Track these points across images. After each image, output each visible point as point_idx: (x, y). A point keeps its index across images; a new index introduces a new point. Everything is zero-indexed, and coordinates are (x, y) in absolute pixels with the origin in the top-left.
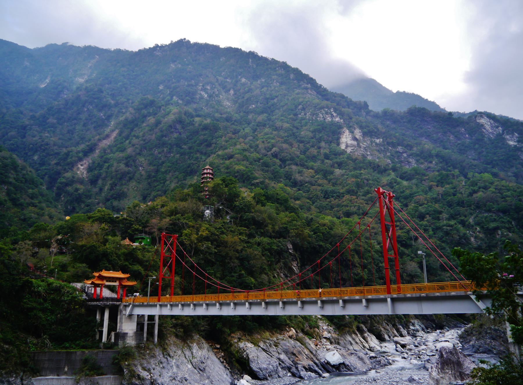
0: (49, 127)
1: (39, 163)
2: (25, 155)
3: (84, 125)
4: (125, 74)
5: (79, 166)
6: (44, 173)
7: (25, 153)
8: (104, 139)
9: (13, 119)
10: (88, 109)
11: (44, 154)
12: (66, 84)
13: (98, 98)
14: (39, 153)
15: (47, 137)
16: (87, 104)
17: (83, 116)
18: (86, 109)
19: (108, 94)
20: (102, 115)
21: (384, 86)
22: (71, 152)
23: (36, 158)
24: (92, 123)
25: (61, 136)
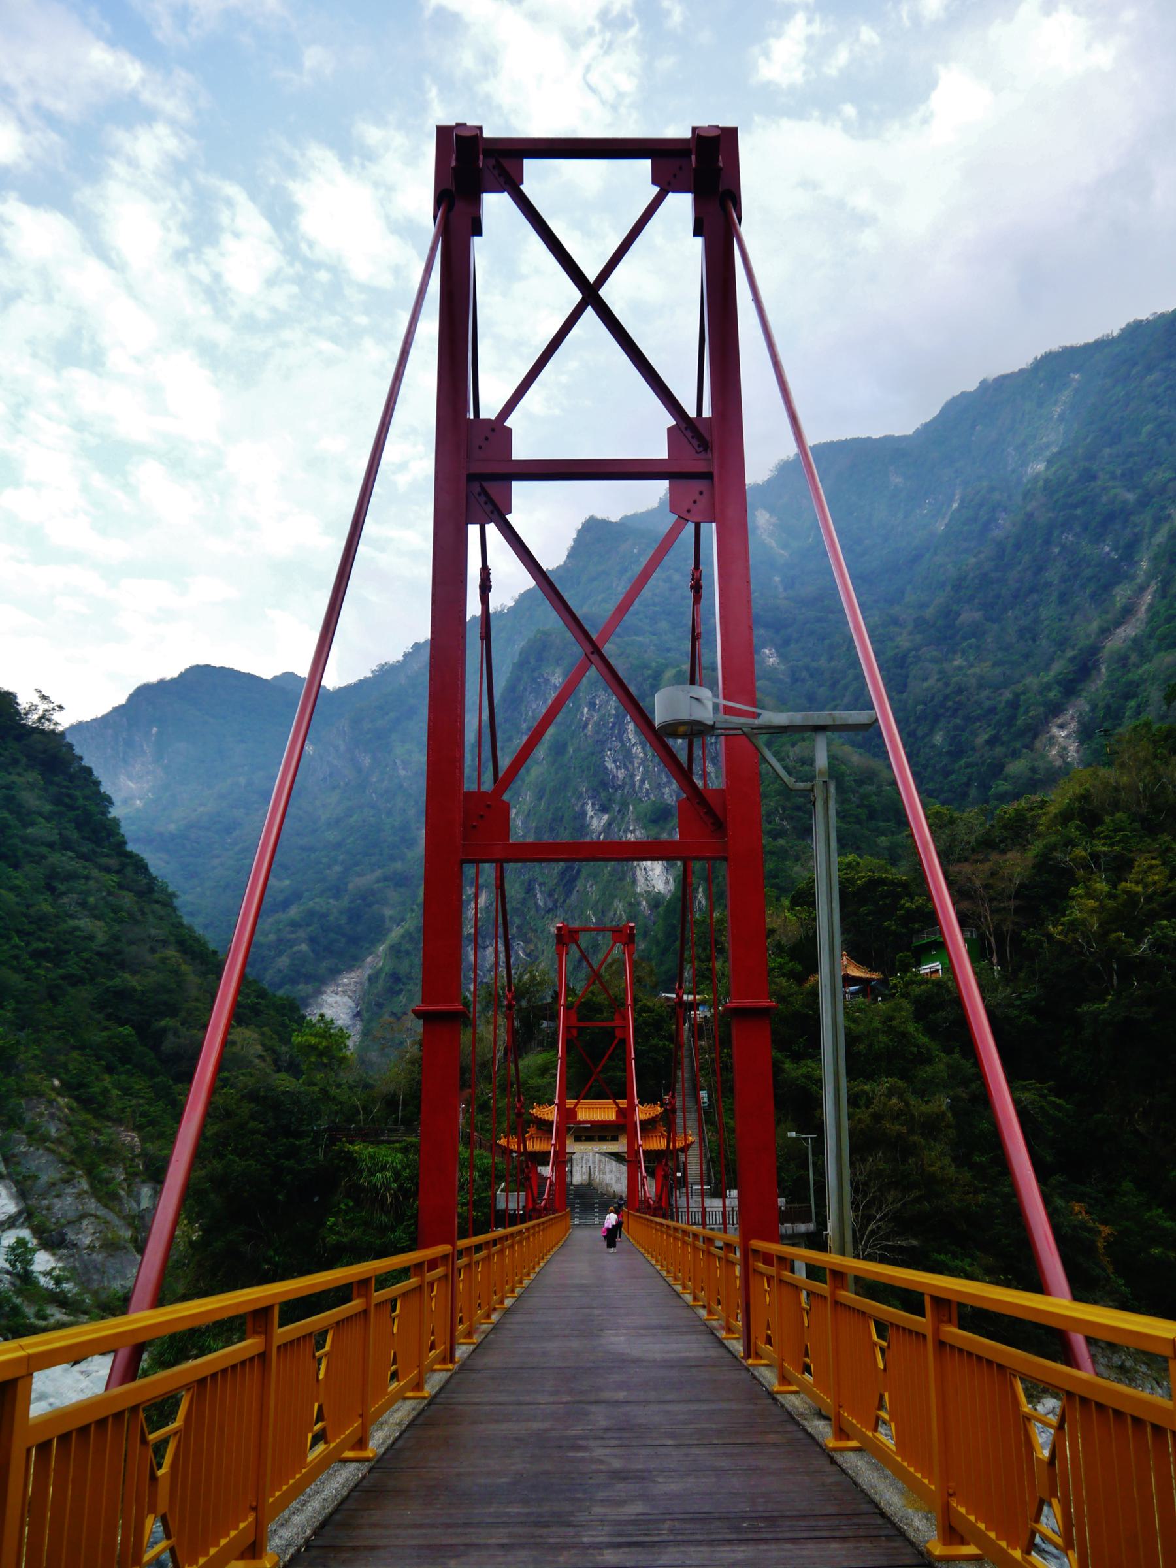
0: (965, 638)
1: (949, 753)
3: (1063, 599)
4: (1160, 390)
5: (1055, 731)
6: (965, 779)
8: (1118, 624)
10: (1063, 547)
11: (958, 721)
12: (996, 496)
13: (1084, 502)
14: (943, 723)
15: (960, 668)
16: (1056, 533)
17: (1052, 575)
18: (1057, 550)
19: (1113, 477)
20: (1107, 549)
21: (876, 435)
22: (1023, 693)
23: (938, 738)
24: (1083, 587)
25: (1000, 655)
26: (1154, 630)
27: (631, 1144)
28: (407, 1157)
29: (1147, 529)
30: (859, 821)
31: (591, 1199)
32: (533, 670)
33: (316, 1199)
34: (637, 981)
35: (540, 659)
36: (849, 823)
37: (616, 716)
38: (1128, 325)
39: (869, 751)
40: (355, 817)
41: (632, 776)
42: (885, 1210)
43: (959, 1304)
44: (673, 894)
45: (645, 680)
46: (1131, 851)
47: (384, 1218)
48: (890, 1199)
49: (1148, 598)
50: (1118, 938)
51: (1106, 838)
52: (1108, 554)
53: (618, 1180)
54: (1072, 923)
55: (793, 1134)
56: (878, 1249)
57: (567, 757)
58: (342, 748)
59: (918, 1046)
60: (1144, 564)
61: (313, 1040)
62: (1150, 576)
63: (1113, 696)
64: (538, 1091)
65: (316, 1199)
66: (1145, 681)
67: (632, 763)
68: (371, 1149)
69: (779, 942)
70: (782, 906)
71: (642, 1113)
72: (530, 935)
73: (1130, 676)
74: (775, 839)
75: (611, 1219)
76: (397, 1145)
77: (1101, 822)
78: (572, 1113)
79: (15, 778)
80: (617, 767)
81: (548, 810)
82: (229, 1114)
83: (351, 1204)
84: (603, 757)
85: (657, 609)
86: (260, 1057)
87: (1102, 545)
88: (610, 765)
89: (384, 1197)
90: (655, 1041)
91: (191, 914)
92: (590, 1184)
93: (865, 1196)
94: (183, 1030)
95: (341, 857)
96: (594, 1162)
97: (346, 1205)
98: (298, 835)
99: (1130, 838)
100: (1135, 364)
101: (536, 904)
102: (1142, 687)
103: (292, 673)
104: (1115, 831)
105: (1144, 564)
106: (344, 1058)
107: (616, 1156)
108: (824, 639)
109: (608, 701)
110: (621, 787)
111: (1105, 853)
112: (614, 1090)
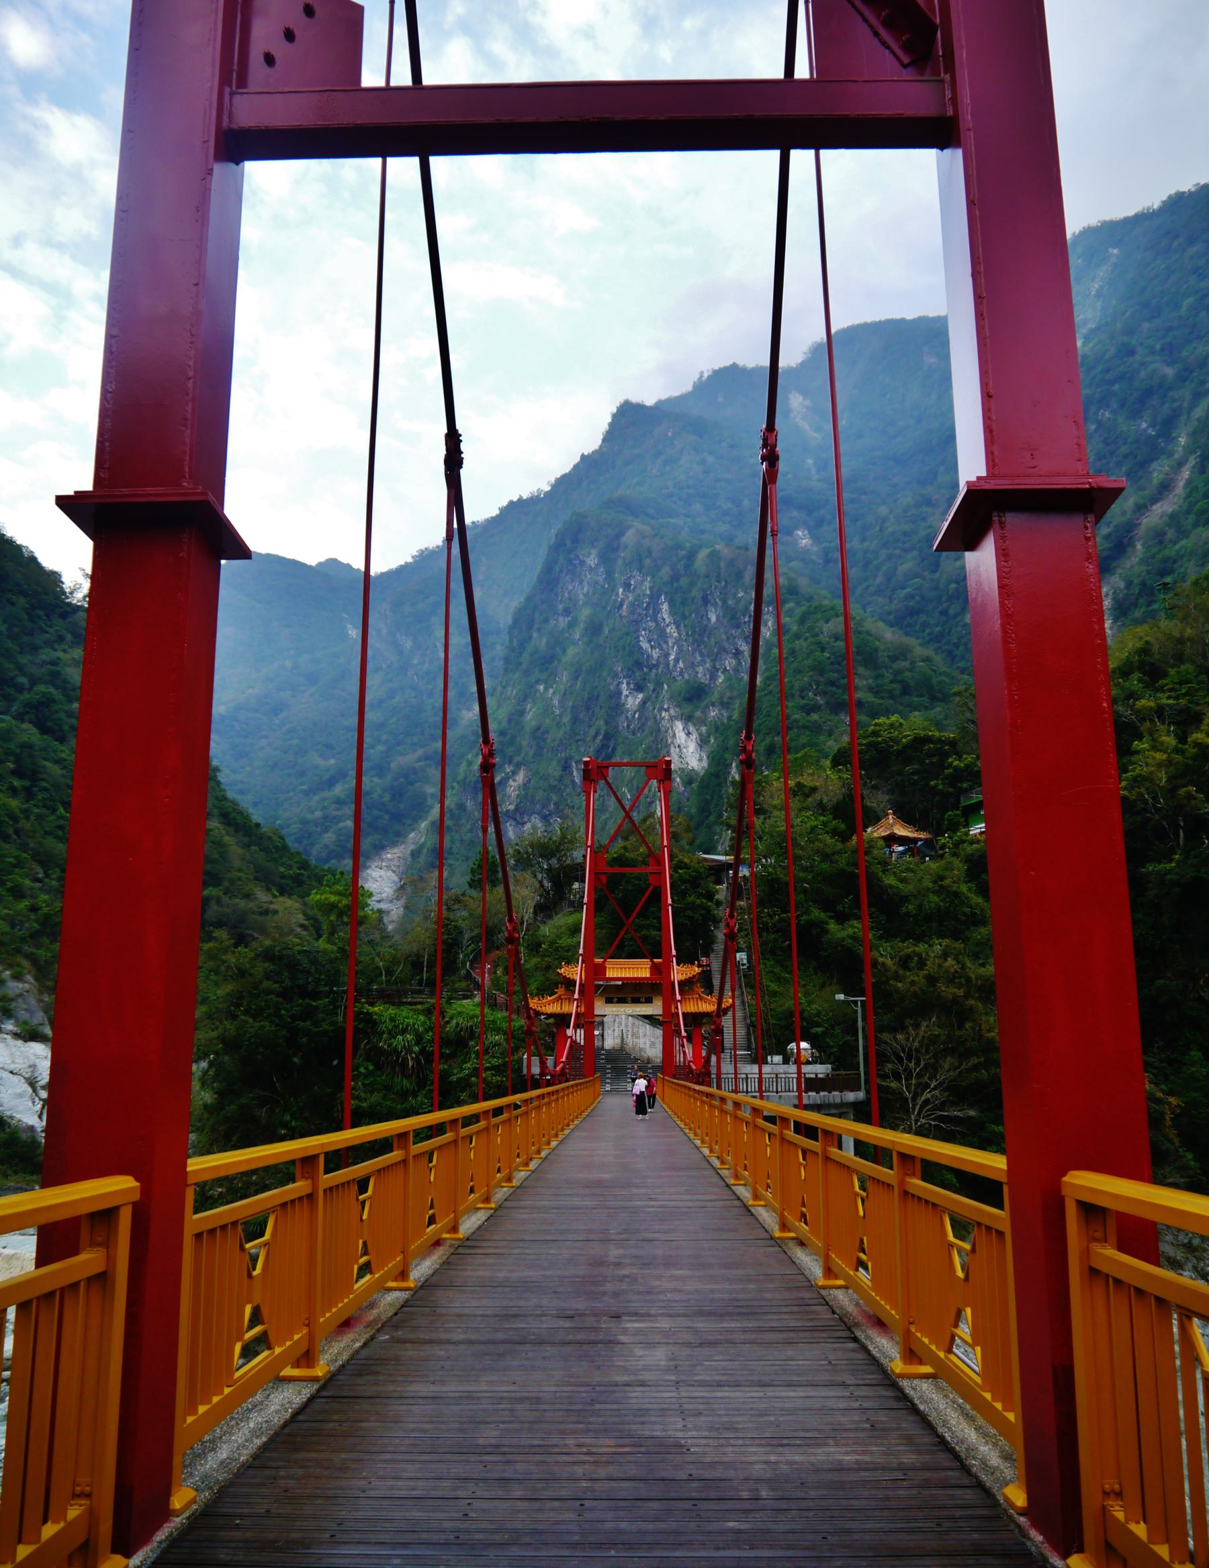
2: (944, 618)
7: (942, 613)
8: (1154, 500)
9: (906, 527)
10: (1100, 424)
13: (1121, 377)
16: (1093, 409)
18: (1093, 427)
19: (1152, 352)
20: (1144, 425)
21: (910, 316)
24: (1119, 464)
26: (1192, 505)
27: (666, 1007)
28: (430, 1019)
29: (1185, 405)
30: (892, 697)
31: (621, 1064)
32: (569, 552)
33: (335, 1063)
34: (674, 837)
35: (576, 541)
36: (883, 698)
37: (651, 597)
38: (1170, 197)
39: (901, 629)
40: (398, 698)
41: (667, 655)
42: (941, 1077)
43: (923, 1160)
44: (707, 771)
45: (679, 560)
46: (1198, 704)
47: (405, 1081)
48: (947, 1066)
49: (1186, 474)
50: (1188, 792)
51: (1170, 690)
52: (1145, 430)
53: (653, 1044)
54: (1135, 779)
55: (841, 997)
56: (933, 1120)
57: (603, 636)
58: (384, 632)
59: (971, 907)
60: (1182, 440)
61: (333, 898)
62: (1189, 451)
63: (1149, 572)
64: (568, 951)
65: (335, 1063)
66: (1182, 557)
67: (666, 642)
68: (392, 1011)
69: (821, 800)
70: (821, 767)
71: (679, 973)
72: (567, 811)
73: (1167, 552)
74: (808, 714)
75: (641, 1084)
76: (419, 1007)
77: (1165, 675)
78: (602, 969)
79: (60, 654)
80: (652, 647)
81: (584, 690)
82: (242, 973)
83: (371, 1068)
84: (638, 637)
85: (691, 491)
86: (302, 926)
87: (1139, 422)
88: (645, 645)
89: (405, 1061)
90: (690, 899)
91: (241, 792)
92: (622, 1049)
93: (918, 1064)
94: (225, 899)
95: (384, 737)
96: (627, 1026)
97: (366, 1068)
98: (342, 716)
99: (1197, 690)
100: (1177, 236)
101: (573, 781)
102: (1179, 563)
103: (336, 560)
104: (1181, 683)
105: (1182, 440)
106: (366, 917)
107: (650, 1019)
108: (857, 520)
109: (642, 581)
110: (656, 666)
111: (1169, 705)
112: (652, 949)
